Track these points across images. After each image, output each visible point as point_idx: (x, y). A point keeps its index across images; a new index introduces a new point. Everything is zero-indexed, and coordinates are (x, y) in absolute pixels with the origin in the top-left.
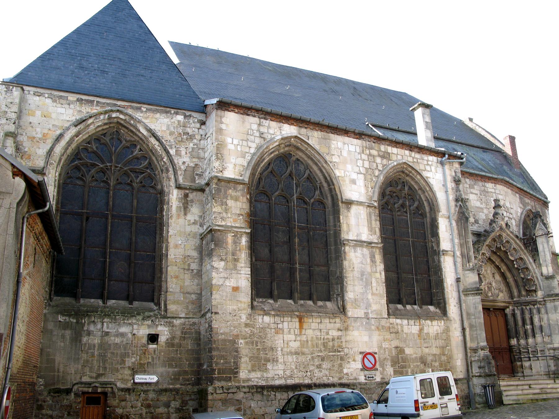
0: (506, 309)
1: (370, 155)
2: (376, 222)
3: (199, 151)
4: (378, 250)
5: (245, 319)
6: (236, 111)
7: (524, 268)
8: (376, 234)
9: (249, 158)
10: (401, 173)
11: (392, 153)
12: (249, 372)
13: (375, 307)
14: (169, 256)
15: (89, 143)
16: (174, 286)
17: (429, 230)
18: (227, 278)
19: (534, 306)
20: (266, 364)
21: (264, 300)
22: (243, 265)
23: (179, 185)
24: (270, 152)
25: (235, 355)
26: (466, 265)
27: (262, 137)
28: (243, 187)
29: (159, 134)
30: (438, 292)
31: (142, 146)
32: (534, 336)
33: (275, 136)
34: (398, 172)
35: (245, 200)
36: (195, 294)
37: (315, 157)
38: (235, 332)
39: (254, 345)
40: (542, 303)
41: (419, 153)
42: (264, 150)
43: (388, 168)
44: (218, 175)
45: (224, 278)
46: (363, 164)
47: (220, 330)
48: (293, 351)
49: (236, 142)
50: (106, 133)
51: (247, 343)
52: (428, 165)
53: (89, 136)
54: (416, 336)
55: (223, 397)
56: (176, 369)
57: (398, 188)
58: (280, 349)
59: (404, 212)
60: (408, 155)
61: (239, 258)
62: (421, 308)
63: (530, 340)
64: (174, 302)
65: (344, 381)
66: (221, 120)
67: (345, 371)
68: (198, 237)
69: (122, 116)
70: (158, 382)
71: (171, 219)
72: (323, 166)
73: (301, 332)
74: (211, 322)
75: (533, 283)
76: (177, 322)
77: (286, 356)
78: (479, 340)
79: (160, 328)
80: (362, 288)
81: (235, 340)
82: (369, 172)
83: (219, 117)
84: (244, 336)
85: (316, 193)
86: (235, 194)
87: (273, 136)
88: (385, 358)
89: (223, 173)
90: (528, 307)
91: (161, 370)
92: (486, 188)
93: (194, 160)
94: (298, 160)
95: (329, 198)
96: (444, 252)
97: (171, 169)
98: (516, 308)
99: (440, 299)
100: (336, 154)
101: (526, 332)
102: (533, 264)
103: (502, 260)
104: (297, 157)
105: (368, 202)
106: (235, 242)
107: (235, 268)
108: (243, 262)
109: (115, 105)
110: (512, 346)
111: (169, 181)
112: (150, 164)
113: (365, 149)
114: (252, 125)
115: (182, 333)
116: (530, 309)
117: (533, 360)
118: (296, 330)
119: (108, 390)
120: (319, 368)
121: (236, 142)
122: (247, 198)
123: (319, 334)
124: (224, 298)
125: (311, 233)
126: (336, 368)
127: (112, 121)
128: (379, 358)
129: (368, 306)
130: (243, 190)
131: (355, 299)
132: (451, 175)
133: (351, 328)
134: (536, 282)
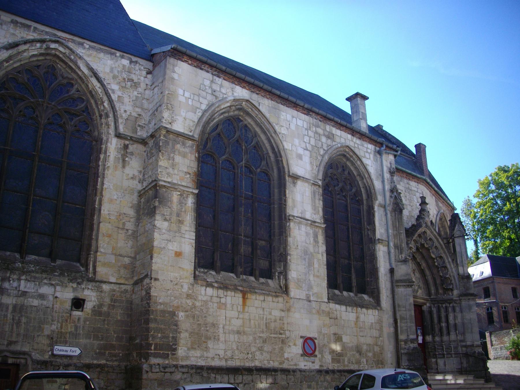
0: (423, 306)
1: (316, 133)
2: (319, 201)
3: (143, 101)
4: (320, 231)
5: (187, 289)
6: (190, 62)
7: (443, 267)
8: (319, 214)
9: (200, 114)
10: (342, 157)
11: (336, 135)
12: (189, 349)
13: (315, 290)
14: (102, 211)
15: (19, 72)
16: (105, 246)
17: (365, 217)
18: (170, 241)
19: (450, 304)
20: (206, 342)
21: (206, 271)
22: (187, 228)
23: (120, 134)
24: (221, 112)
25: (174, 329)
26: (399, 256)
27: (214, 95)
28: (192, 144)
29: (101, 75)
30: (372, 281)
31: (81, 85)
32: (448, 334)
33: (227, 96)
34: (339, 155)
35: (193, 158)
36: (128, 257)
37: (265, 125)
38: (175, 303)
39: (195, 319)
40: (458, 302)
41: (360, 139)
42: (215, 108)
43: (333, 149)
44: (167, 126)
45: (167, 240)
46: (310, 140)
47: (159, 299)
48: (235, 329)
49: (187, 94)
50: (40, 65)
51: (187, 316)
52: (367, 152)
53: (21, 65)
54: (353, 325)
55: (159, 377)
56: (102, 342)
57: (339, 171)
58: (221, 326)
59: (343, 196)
60: (350, 140)
61: (183, 220)
62: (356, 295)
63: (445, 338)
64: (104, 264)
65: (285, 366)
66: (174, 69)
67: (286, 355)
68: (136, 194)
69: (61, 49)
70: (80, 356)
71: (108, 170)
72: (271, 136)
73: (244, 309)
74: (150, 288)
75: (449, 282)
76: (105, 287)
77: (227, 335)
78: (409, 333)
79: (87, 292)
80: (305, 268)
81: (175, 312)
82: (313, 150)
83: (172, 66)
84: (185, 308)
85: (263, 163)
86: (184, 150)
87: (225, 96)
88: (324, 345)
89: (172, 125)
90: (444, 305)
91: (83, 341)
92: (410, 186)
93: (137, 110)
94: (246, 126)
95: (275, 171)
96: (380, 241)
97: (111, 115)
98: (432, 305)
99: (374, 288)
100: (285, 126)
101: (441, 329)
102: (451, 263)
103: (423, 257)
104: (246, 122)
105: (313, 179)
106: (180, 203)
107: (179, 231)
108: (188, 225)
109: (55, 35)
110: (428, 343)
111: (109, 128)
112: (87, 108)
113: (312, 126)
114: (205, 80)
115: (112, 300)
116: (446, 307)
117: (447, 357)
118: (239, 306)
119: (20, 362)
120: (260, 350)
121: (187, 94)
122: (195, 157)
123: (261, 312)
124: (166, 263)
125: (256, 204)
126: (277, 351)
127: (49, 52)
128: (319, 344)
129: (310, 287)
130: (192, 147)
131: (298, 279)
132: (387, 167)
133: (293, 310)
134: (453, 282)
